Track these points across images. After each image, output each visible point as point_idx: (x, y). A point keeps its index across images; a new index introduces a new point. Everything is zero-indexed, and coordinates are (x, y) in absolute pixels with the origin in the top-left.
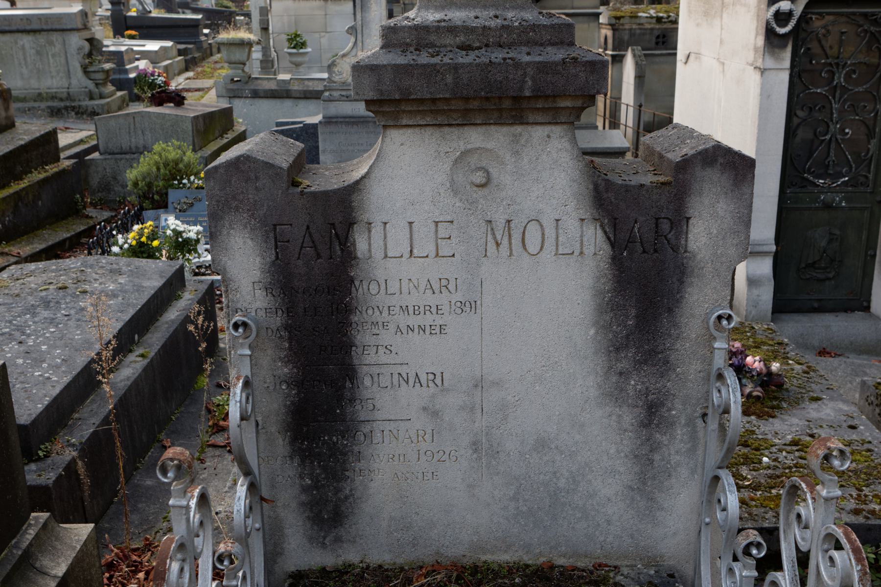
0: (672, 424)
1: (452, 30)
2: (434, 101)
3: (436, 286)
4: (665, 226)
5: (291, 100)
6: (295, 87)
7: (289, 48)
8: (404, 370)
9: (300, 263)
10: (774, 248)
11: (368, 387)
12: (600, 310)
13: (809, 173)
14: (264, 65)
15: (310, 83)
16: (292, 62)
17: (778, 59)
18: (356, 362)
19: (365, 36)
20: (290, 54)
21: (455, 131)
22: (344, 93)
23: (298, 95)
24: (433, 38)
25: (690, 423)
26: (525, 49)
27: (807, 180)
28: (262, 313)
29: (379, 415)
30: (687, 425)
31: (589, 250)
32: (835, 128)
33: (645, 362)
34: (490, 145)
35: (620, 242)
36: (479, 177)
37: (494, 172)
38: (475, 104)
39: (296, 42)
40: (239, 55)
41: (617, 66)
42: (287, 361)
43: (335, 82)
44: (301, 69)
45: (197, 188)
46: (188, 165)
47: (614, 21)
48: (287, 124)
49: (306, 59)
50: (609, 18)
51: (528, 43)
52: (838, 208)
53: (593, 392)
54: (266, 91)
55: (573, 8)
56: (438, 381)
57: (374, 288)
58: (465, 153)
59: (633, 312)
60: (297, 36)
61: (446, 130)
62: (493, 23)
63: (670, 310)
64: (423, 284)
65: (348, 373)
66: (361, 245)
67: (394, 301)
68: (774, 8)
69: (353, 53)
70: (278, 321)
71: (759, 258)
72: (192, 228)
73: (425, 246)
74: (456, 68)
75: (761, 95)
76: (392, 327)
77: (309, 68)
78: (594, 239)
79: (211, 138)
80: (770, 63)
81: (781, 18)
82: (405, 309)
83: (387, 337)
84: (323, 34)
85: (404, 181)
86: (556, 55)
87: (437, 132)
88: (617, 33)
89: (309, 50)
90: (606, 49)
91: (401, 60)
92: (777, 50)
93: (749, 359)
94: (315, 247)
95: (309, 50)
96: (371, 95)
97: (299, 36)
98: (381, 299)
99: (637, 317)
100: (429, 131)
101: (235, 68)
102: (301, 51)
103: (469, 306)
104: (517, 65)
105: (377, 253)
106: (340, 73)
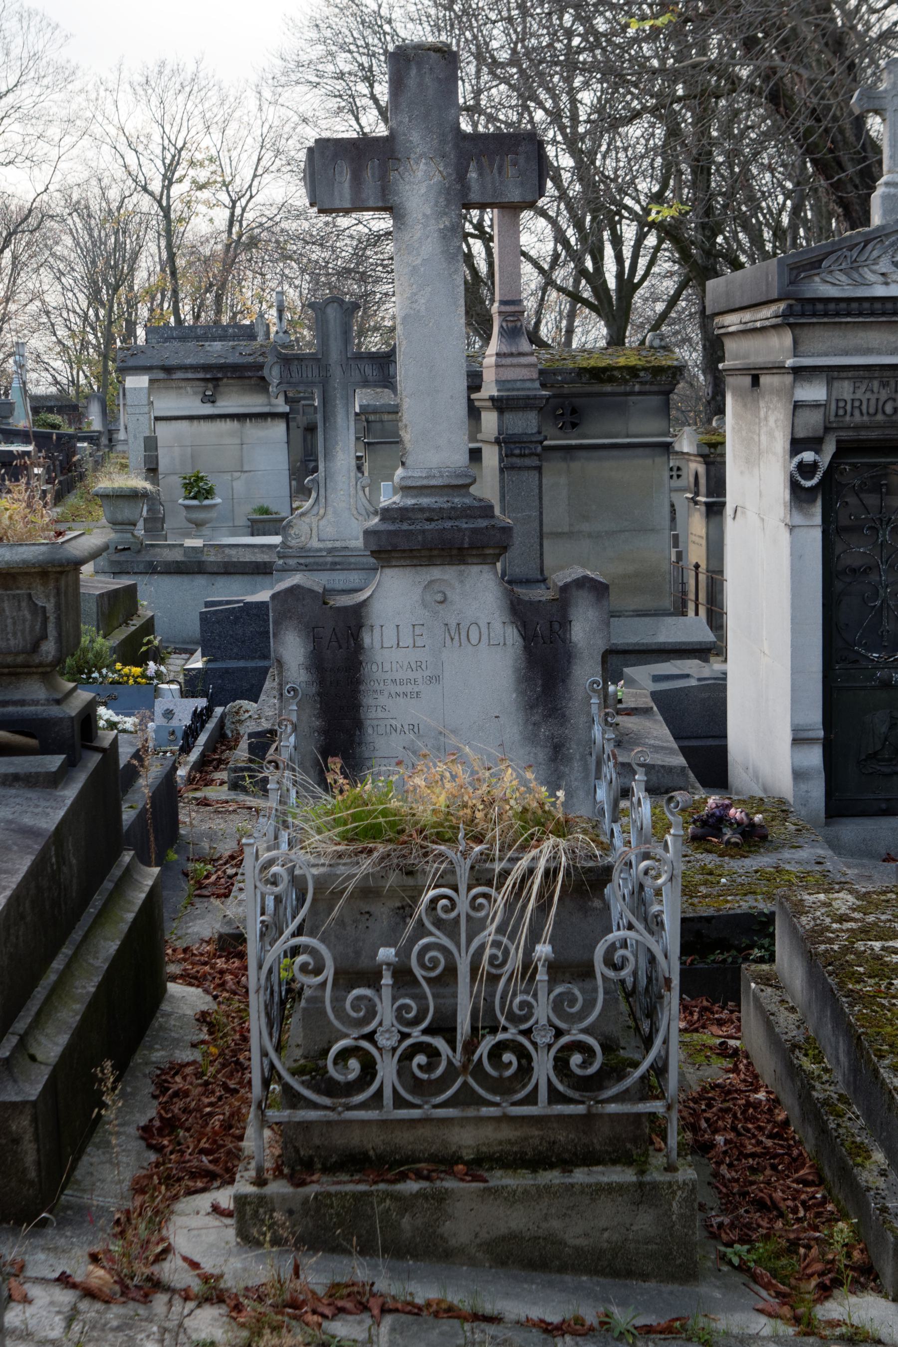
0: (571, 759)
1: (422, 510)
2: (411, 550)
3: (414, 666)
4: (556, 626)
5: (205, 576)
6: (211, 557)
7: (186, 498)
8: (394, 722)
9: (329, 652)
10: (821, 734)
13: (860, 645)
14: (149, 526)
15: (233, 552)
16: (190, 521)
18: (363, 717)
19: (329, 491)
20: (187, 507)
21: (424, 569)
22: (302, 561)
23: (215, 570)
24: (410, 515)
25: (583, 758)
26: (464, 520)
27: (858, 652)
28: (303, 685)
29: (377, 754)
30: (581, 760)
31: (509, 642)
32: (886, 592)
33: (550, 716)
34: (445, 577)
35: (529, 638)
36: (439, 597)
37: (449, 594)
38: (435, 553)
39: (198, 488)
43: (291, 548)
44: (206, 531)
45: (111, 683)
46: (98, 655)
47: (706, 450)
48: (220, 603)
49: (213, 514)
50: (698, 446)
51: (467, 516)
54: (168, 564)
55: (628, 436)
56: (416, 730)
57: (374, 668)
58: (431, 582)
59: (540, 682)
60: (199, 479)
61: (419, 568)
62: (445, 506)
63: (563, 681)
64: (406, 664)
65: (358, 724)
66: (367, 640)
67: (387, 676)
68: (797, 459)
69: (314, 511)
70: (313, 689)
71: (805, 746)
72: (126, 719)
74: (423, 532)
75: (791, 555)
76: (386, 693)
77: (214, 528)
78: (512, 635)
79: (115, 624)
80: (798, 519)
81: (806, 470)
82: (394, 681)
83: (382, 700)
84: (236, 474)
85: (395, 601)
86: (482, 523)
87: (413, 570)
88: (712, 468)
89: (218, 500)
90: (697, 494)
91: (391, 527)
92: (805, 505)
93: (732, 811)
94: (338, 641)
95: (218, 500)
96: (374, 548)
97: (202, 479)
99: (542, 685)
100: (409, 569)
101: (121, 531)
102: (206, 502)
103: (435, 679)
104: (460, 530)
105: (377, 645)
106: (298, 536)
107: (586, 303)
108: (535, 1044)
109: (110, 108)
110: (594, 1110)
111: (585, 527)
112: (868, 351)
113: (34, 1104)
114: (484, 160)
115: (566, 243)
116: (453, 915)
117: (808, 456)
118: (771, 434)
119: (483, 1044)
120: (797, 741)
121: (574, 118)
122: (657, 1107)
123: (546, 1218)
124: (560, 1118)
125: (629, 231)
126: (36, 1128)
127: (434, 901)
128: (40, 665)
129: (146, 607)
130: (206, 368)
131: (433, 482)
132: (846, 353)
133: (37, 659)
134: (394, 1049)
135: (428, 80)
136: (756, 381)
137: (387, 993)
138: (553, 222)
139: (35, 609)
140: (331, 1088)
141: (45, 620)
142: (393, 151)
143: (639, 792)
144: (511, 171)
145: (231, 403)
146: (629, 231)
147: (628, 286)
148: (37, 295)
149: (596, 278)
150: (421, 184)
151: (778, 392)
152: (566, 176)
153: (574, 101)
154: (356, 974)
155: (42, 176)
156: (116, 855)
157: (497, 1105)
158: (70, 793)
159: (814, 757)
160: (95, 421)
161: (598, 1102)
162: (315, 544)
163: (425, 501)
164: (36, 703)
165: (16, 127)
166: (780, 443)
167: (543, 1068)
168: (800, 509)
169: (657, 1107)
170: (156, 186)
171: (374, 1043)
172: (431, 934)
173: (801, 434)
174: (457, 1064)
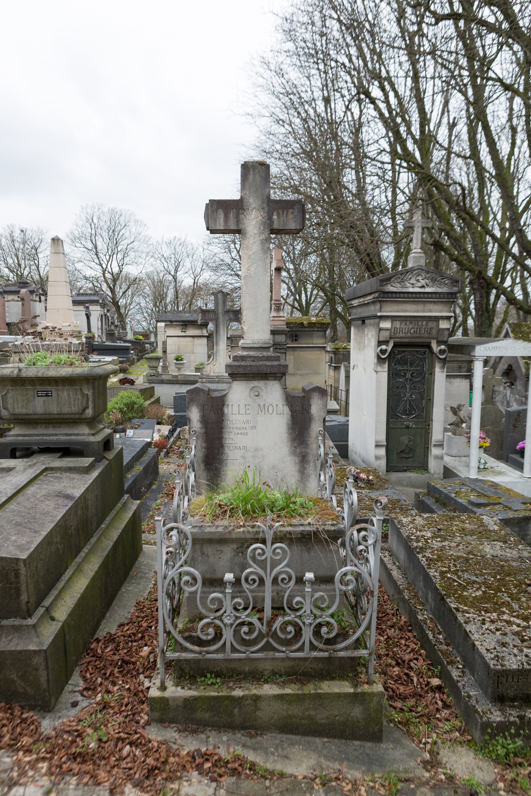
1: (250, 357)
11: (227, 450)
12: (289, 429)
17: (383, 368)
25: (314, 461)
36: (257, 394)
40: (154, 364)
41: (337, 372)
42: (205, 442)
52: (412, 428)
53: (287, 452)
65: (222, 446)
66: (226, 411)
70: (203, 431)
73: (243, 411)
78: (286, 410)
80: (379, 369)
81: (383, 352)
83: (232, 436)
98: (231, 425)
105: (230, 413)
107: (296, 308)
108: (304, 623)
109: (159, 249)
110: (332, 656)
111: (299, 372)
112: (406, 311)
113: (45, 651)
114: (280, 211)
115: (291, 291)
116: (263, 557)
117: (384, 347)
118: (369, 340)
119: (277, 622)
120: (377, 446)
121: (294, 254)
122: (363, 652)
123: (307, 709)
124: (315, 659)
125: (309, 286)
126: (47, 663)
127: (255, 549)
128: (86, 419)
129: (157, 394)
130: (183, 321)
131: (255, 346)
132: (398, 311)
133: (84, 416)
134: (232, 625)
135: (257, 176)
136: (363, 322)
137: (229, 597)
138: (287, 284)
139: (83, 395)
140: (200, 643)
141: (88, 399)
142: (242, 206)
143: (350, 487)
144: (290, 216)
145: (191, 332)
146: (309, 286)
147: (308, 304)
148: (139, 304)
149: (300, 302)
150: (253, 221)
151: (373, 325)
152: (291, 272)
153: (294, 249)
154: (213, 582)
155: (140, 268)
156: (122, 496)
157: (284, 652)
158: (95, 474)
159: (382, 452)
160: (152, 339)
161: (334, 651)
162: (212, 374)
163: (252, 353)
164: (83, 435)
165: (133, 254)
166: (373, 342)
167: (307, 634)
168: (380, 365)
169: (363, 652)
170: (173, 273)
171: (222, 621)
172: (251, 566)
173: (381, 339)
174: (264, 632)
